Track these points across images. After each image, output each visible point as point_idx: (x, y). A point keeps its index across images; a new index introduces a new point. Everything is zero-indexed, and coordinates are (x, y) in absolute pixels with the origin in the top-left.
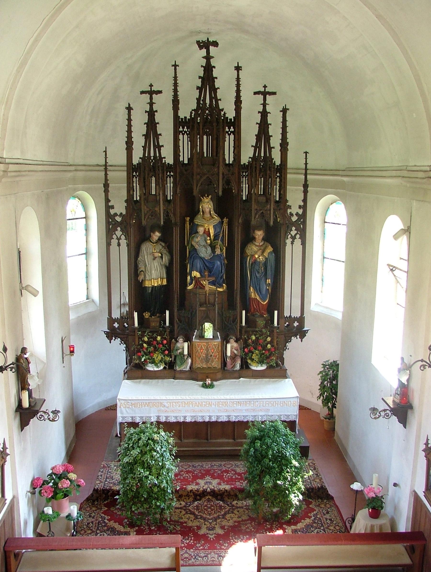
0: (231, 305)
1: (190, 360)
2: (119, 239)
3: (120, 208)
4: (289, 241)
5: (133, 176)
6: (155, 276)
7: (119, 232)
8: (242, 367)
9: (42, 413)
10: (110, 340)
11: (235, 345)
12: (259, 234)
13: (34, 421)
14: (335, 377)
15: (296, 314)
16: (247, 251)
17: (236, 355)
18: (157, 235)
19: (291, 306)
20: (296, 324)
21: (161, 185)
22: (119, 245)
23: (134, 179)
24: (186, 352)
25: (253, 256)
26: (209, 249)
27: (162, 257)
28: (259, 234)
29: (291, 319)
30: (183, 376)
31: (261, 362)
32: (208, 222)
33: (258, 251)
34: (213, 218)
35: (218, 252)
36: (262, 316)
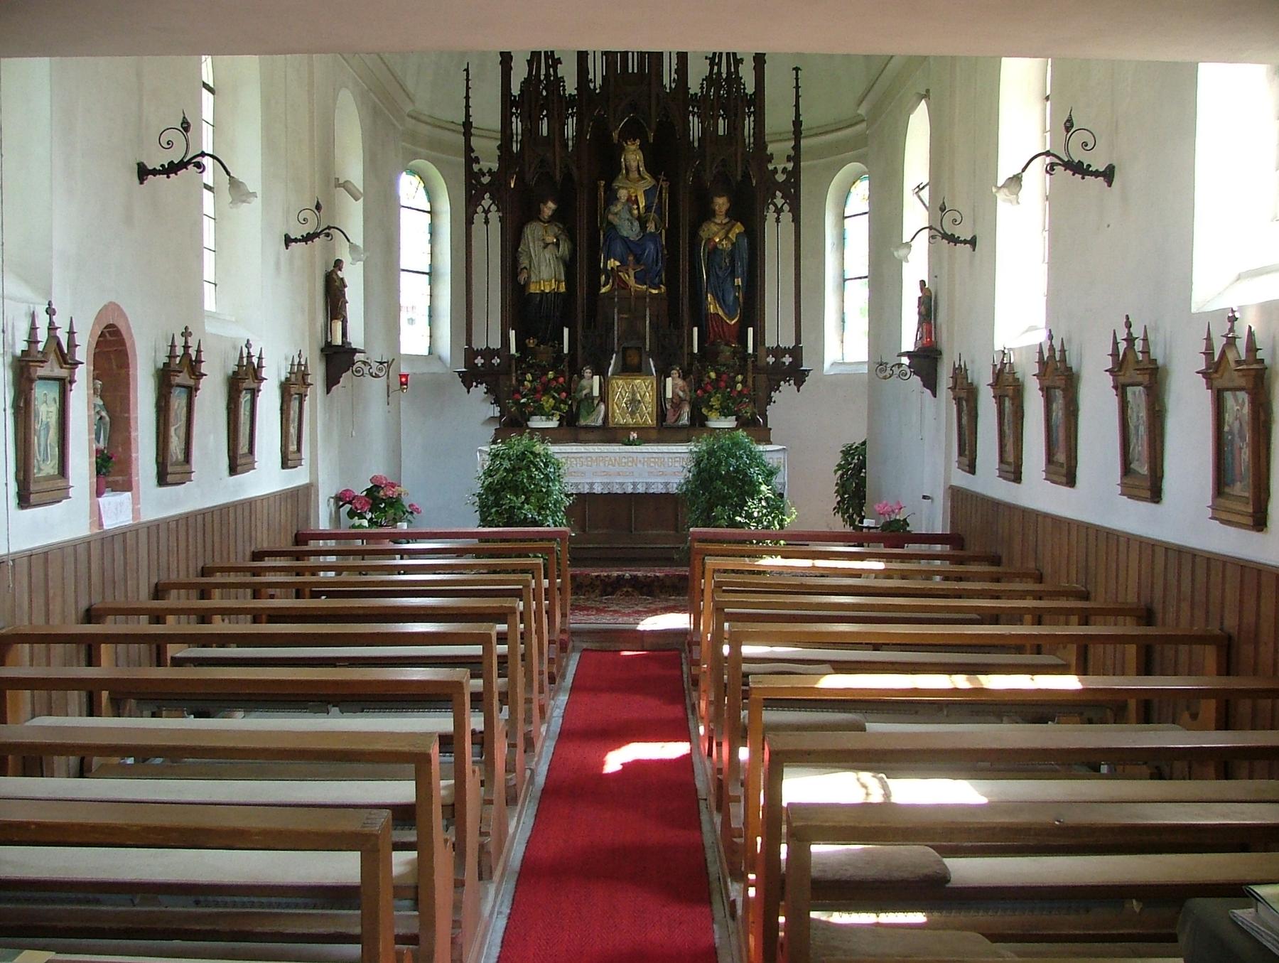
0: (673, 317)
1: (603, 407)
2: (486, 212)
3: (489, 162)
4: (771, 216)
5: (512, 114)
6: (546, 276)
7: (487, 202)
8: (692, 418)
9: (359, 364)
10: (469, 387)
11: (680, 382)
12: (721, 203)
13: (346, 378)
14: (862, 465)
15: (788, 342)
16: (701, 233)
17: (681, 400)
18: (549, 208)
19: (778, 332)
20: (787, 360)
21: (558, 125)
22: (487, 222)
23: (514, 119)
24: (596, 393)
25: (709, 240)
26: (636, 224)
27: (557, 245)
28: (721, 203)
29: (778, 352)
30: (590, 436)
31: (725, 412)
32: (634, 193)
33: (720, 233)
34: (643, 179)
35: (651, 227)
36: (728, 344)
